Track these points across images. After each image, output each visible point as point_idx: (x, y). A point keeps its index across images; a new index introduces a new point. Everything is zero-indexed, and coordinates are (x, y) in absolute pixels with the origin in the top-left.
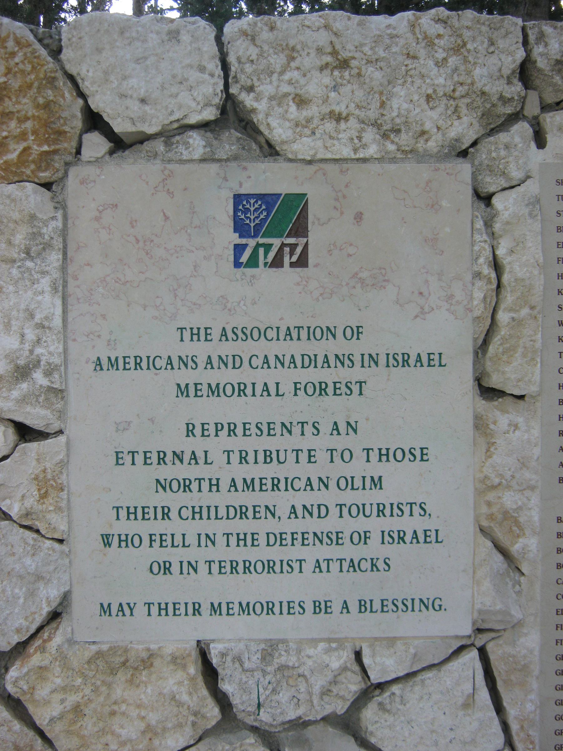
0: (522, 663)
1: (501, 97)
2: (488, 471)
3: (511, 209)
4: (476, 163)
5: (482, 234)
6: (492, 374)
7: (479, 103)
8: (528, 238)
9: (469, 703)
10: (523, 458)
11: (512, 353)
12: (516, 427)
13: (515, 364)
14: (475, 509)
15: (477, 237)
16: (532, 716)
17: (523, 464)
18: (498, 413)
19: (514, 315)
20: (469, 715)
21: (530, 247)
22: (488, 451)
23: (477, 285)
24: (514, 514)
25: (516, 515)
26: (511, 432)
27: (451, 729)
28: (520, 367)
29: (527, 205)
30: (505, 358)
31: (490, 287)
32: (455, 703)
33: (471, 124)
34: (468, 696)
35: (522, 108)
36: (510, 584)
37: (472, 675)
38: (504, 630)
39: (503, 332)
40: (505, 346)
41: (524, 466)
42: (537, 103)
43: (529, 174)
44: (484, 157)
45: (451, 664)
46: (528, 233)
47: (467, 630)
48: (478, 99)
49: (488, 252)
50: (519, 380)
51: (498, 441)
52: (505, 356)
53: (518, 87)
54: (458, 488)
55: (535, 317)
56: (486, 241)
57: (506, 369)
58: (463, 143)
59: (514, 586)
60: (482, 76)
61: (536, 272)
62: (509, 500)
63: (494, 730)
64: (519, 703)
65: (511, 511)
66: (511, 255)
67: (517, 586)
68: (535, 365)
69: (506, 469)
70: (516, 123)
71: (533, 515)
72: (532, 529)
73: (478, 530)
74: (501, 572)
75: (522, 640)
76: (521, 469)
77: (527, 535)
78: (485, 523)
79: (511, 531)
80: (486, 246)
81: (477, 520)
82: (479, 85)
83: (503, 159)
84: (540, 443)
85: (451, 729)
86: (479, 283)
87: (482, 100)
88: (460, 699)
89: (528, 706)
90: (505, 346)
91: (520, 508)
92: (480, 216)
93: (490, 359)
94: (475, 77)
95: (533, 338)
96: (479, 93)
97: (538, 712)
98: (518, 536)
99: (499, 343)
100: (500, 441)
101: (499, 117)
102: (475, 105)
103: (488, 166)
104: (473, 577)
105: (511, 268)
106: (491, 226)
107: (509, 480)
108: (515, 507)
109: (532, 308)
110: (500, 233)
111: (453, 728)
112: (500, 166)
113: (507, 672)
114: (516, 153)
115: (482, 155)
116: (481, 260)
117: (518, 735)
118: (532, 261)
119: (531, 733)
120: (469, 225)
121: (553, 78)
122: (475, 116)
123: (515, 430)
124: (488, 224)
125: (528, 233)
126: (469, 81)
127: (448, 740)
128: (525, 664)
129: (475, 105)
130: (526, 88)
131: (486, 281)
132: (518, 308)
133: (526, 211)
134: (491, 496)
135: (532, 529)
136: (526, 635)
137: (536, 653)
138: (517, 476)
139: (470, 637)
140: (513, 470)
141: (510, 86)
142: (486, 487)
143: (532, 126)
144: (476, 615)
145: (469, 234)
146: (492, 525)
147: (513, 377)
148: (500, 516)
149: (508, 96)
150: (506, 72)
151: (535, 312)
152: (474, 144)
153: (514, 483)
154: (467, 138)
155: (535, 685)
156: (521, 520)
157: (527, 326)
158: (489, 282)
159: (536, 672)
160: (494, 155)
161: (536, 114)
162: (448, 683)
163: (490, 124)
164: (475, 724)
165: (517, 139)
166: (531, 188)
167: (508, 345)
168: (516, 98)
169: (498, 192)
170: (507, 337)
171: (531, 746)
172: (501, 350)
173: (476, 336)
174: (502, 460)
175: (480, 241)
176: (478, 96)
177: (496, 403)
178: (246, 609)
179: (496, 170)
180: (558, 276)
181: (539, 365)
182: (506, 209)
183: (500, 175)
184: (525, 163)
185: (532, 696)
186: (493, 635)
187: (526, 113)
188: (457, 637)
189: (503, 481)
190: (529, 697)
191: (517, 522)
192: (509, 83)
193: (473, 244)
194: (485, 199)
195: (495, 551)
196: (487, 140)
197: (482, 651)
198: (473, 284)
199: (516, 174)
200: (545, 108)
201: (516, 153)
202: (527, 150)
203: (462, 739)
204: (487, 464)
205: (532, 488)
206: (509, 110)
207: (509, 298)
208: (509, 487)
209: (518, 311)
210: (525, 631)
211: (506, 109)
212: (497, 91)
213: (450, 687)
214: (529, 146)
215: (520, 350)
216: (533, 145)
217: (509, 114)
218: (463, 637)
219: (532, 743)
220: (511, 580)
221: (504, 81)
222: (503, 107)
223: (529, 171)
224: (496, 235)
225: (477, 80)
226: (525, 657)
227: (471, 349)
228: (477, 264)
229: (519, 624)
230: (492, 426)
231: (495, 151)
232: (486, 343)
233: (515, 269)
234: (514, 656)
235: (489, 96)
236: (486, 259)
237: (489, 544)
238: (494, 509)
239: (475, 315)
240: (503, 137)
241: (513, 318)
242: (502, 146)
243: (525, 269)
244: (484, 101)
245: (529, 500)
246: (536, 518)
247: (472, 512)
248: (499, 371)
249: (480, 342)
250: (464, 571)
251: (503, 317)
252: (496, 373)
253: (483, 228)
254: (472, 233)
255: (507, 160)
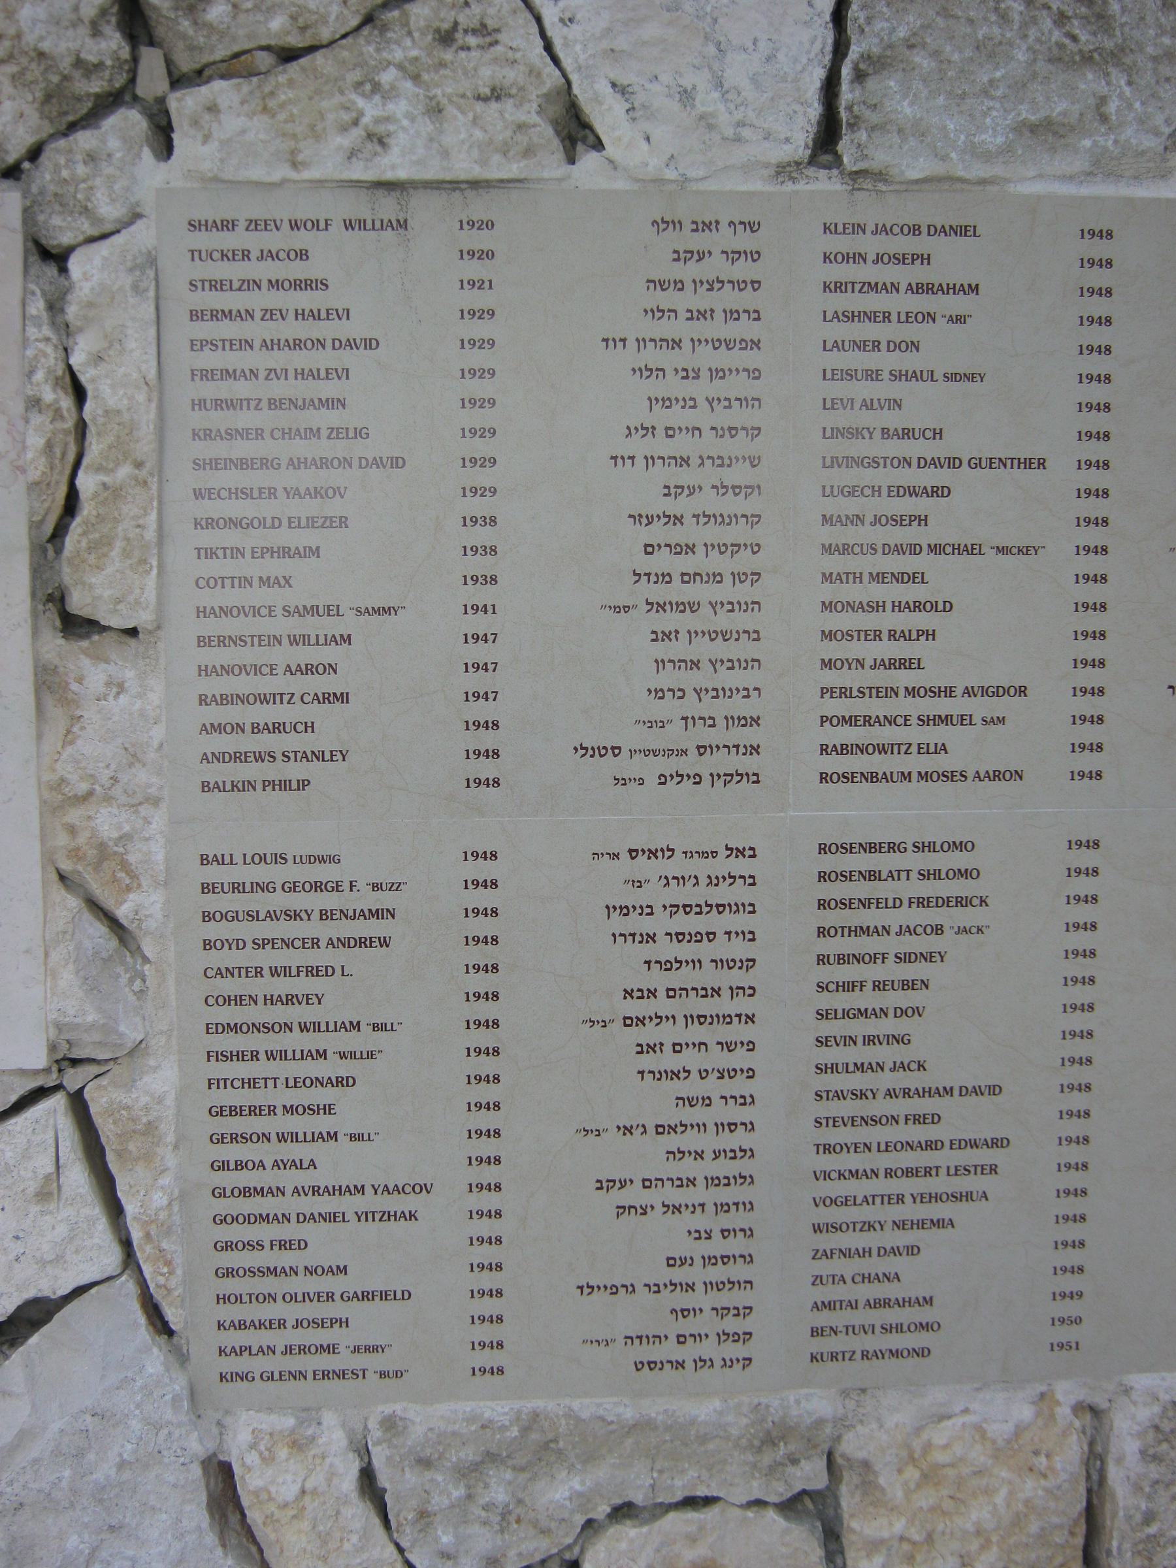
0: (144, 1120)
1: (79, 63)
2: (65, 768)
3: (95, 278)
4: (34, 189)
5: (39, 326)
6: (72, 589)
7: (37, 73)
8: (130, 332)
9: (48, 1191)
10: (133, 745)
11: (105, 549)
12: (121, 688)
13: (109, 570)
14: (43, 838)
15: (32, 332)
16: (163, 1215)
17: (134, 758)
18: (86, 662)
19: (106, 479)
20: (51, 1213)
21: (132, 351)
22: (69, 732)
23: (33, 422)
24: (116, 849)
25: (121, 850)
26: (111, 698)
27: (17, 1238)
28: (118, 576)
29: (131, 270)
30: (92, 559)
31: (59, 425)
32: (23, 1191)
33: (22, 115)
34: (47, 1178)
35: (133, 80)
36: (125, 978)
37: (52, 1141)
38: (114, 1059)
39: (87, 509)
40: (91, 537)
41: (139, 761)
42: (162, 70)
43: (138, 210)
44: (48, 177)
45: (13, 1121)
46: (129, 323)
47: (39, 1059)
48: (34, 66)
49: (52, 358)
50: (119, 601)
51: (86, 715)
52: (93, 556)
53: (113, 43)
54: (10, 799)
55: (145, 482)
56: (48, 339)
57: (93, 580)
58: (7, 152)
59: (131, 981)
60: (35, 22)
61: (141, 397)
62: (107, 822)
63: (96, 1241)
64: (142, 1193)
65: (111, 843)
66: (96, 365)
67: (138, 982)
68: (148, 572)
69: (101, 765)
70: (112, 112)
71: (152, 852)
72: (152, 876)
73: (55, 877)
74: (105, 955)
75: (147, 1079)
76: (131, 765)
77: (146, 888)
78: (66, 866)
79: (115, 880)
80: (49, 350)
81: (48, 858)
82: (30, 39)
83: (84, 181)
84: (164, 719)
85: (17, 1238)
86: (37, 419)
87: (42, 67)
88: (31, 1183)
89: (156, 1197)
90: (91, 537)
91: (125, 838)
92: (38, 292)
93: (70, 561)
94: (22, 24)
95: (141, 522)
96: (33, 54)
97: (176, 1208)
98: (129, 889)
99: (79, 530)
100: (89, 713)
101: (79, 99)
102: (29, 77)
103: (56, 195)
104: (46, 964)
105: (96, 389)
106: (62, 310)
107: (108, 785)
108: (115, 835)
109: (139, 465)
110: (79, 324)
111: (21, 1234)
112: (79, 196)
113: (120, 1136)
114: (109, 170)
115: (44, 175)
116: (39, 376)
117: (144, 1251)
118: (135, 375)
119: (164, 1245)
120: (18, 311)
121: (179, 24)
122: (30, 98)
123: (118, 694)
124: (55, 307)
125: (129, 323)
126: (12, 31)
127: (12, 1256)
128: (149, 1123)
129: (29, 77)
130: (133, 39)
131: (51, 414)
132: (111, 465)
133: (127, 281)
134: (74, 815)
135: (152, 876)
136: (155, 1069)
137: (170, 1101)
138: (124, 778)
139: (47, 1071)
140: (113, 767)
141: (98, 39)
142: (60, 800)
143: (151, 117)
144: (53, 1033)
145: (19, 326)
146: (80, 868)
147: (107, 593)
148: (92, 853)
149: (92, 59)
150: (89, 11)
151: (143, 473)
152: (34, 154)
153: (117, 791)
154: (13, 141)
155: (171, 1161)
156: (132, 858)
157: (130, 499)
158: (58, 415)
159: (170, 1138)
160: (65, 173)
161: (160, 94)
162: (9, 1154)
163: (66, 113)
164: (62, 1230)
165: (113, 143)
166: (141, 236)
167: (97, 535)
168: (109, 63)
169: (80, 245)
170: (93, 520)
171: (165, 1270)
172: (84, 544)
173: (36, 518)
174: (94, 750)
175: (37, 340)
176: (32, 60)
177: (85, 644)
178: (239, 1299)
179: (71, 203)
180: (193, 404)
181: (155, 572)
182: (86, 277)
183: (80, 214)
184: (127, 189)
185: (165, 1180)
186: (94, 1069)
187: (139, 92)
188: (23, 1072)
189: (97, 787)
190: (161, 1182)
191: (125, 865)
192: (96, 32)
193: (25, 343)
194: (54, 257)
195: (87, 916)
196: (53, 146)
197: (79, 1104)
198: (27, 421)
199: (109, 211)
200: (178, 81)
201: (109, 170)
202: (133, 165)
203: (38, 1255)
204: (65, 756)
205: (155, 802)
206: (96, 86)
207: (94, 447)
208: (108, 799)
209: (112, 470)
210: (152, 1063)
211: (92, 84)
212: (68, 49)
213: (12, 1162)
214: (138, 156)
215: (119, 544)
216: (147, 154)
217: (97, 96)
218: (36, 1072)
219: (168, 1263)
220: (126, 971)
221: (84, 31)
222: (84, 81)
223: (138, 204)
224: (72, 328)
225: (26, 29)
226: (147, 1108)
227: (25, 542)
228: (31, 384)
229: (137, 1050)
230: (74, 687)
231: (67, 166)
232: (59, 533)
233: (105, 392)
234: (128, 1108)
235: (53, 59)
236: (49, 372)
237: (74, 902)
238: (82, 839)
239: (30, 479)
240: (84, 139)
241: (104, 484)
242: (79, 157)
243: (121, 393)
244: (46, 70)
245: (149, 823)
246: (160, 857)
247: (37, 845)
248: (83, 583)
249: (49, 529)
250: (27, 952)
251: (86, 482)
252: (79, 586)
253: (45, 315)
254: (24, 325)
255: (90, 183)
